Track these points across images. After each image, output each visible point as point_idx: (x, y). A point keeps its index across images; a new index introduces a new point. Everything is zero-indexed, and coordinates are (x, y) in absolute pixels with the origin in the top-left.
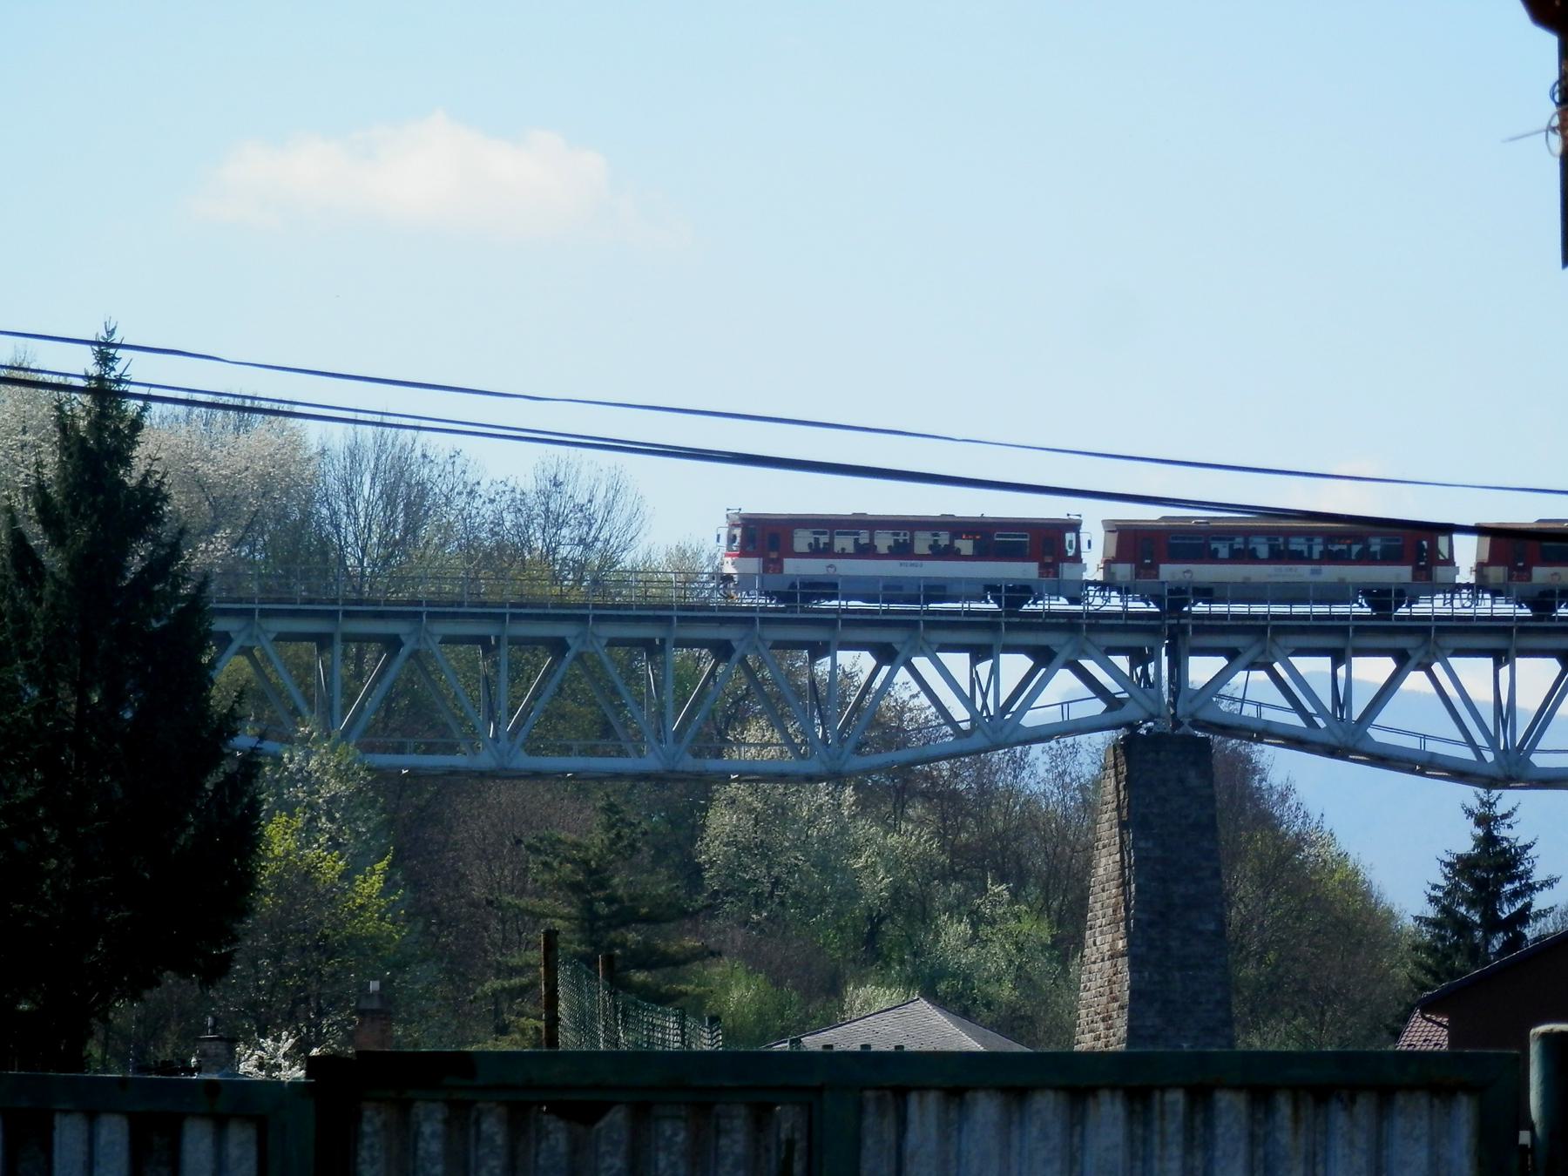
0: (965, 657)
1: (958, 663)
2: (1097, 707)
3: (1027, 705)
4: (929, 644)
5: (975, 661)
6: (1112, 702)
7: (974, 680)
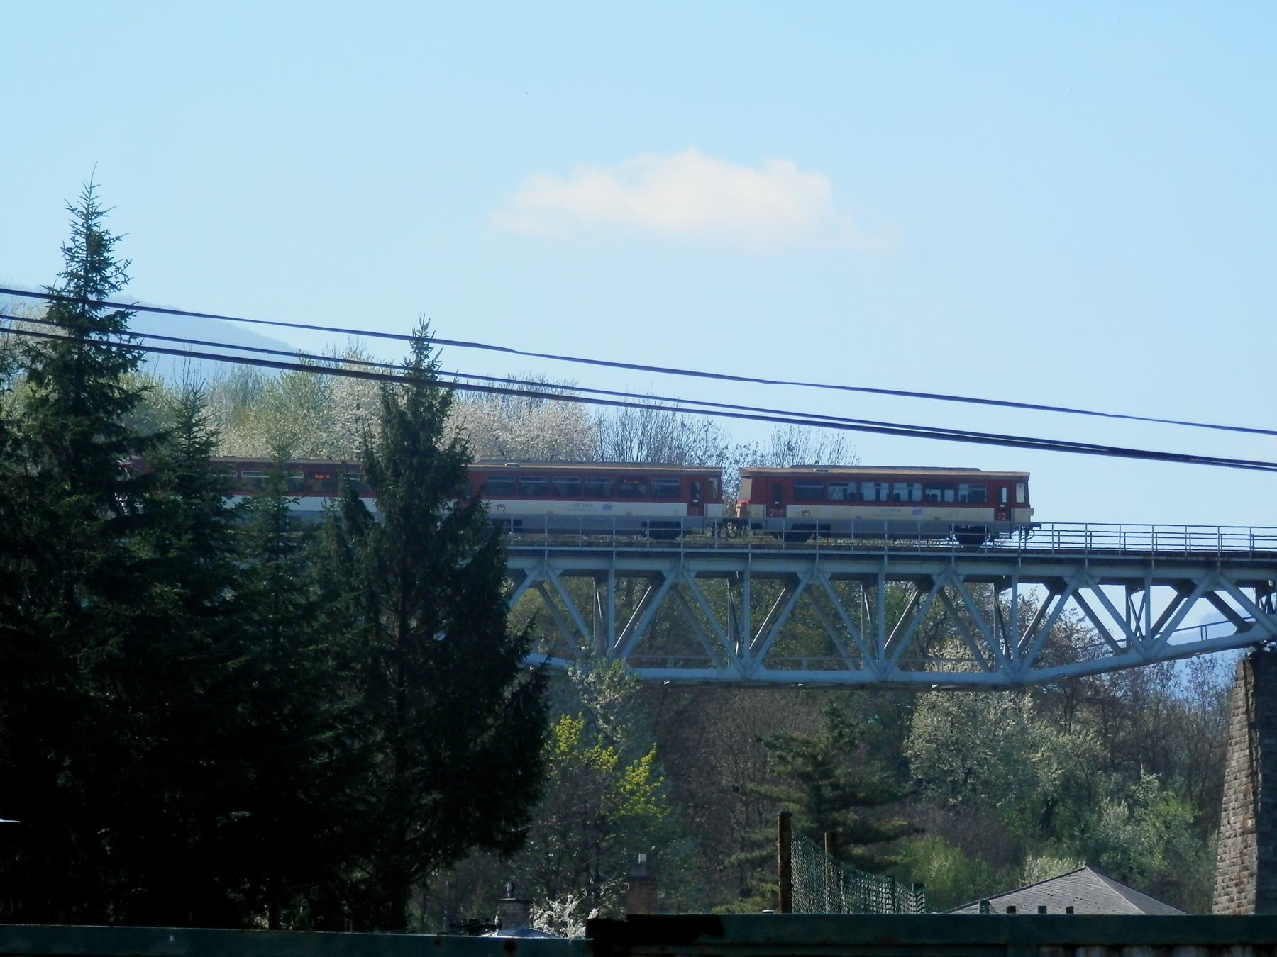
0: (1121, 589)
1: (1116, 593)
2: (1230, 629)
3: (1172, 628)
4: (1092, 577)
5: (1130, 591)
6: (1242, 625)
7: (1129, 607)
